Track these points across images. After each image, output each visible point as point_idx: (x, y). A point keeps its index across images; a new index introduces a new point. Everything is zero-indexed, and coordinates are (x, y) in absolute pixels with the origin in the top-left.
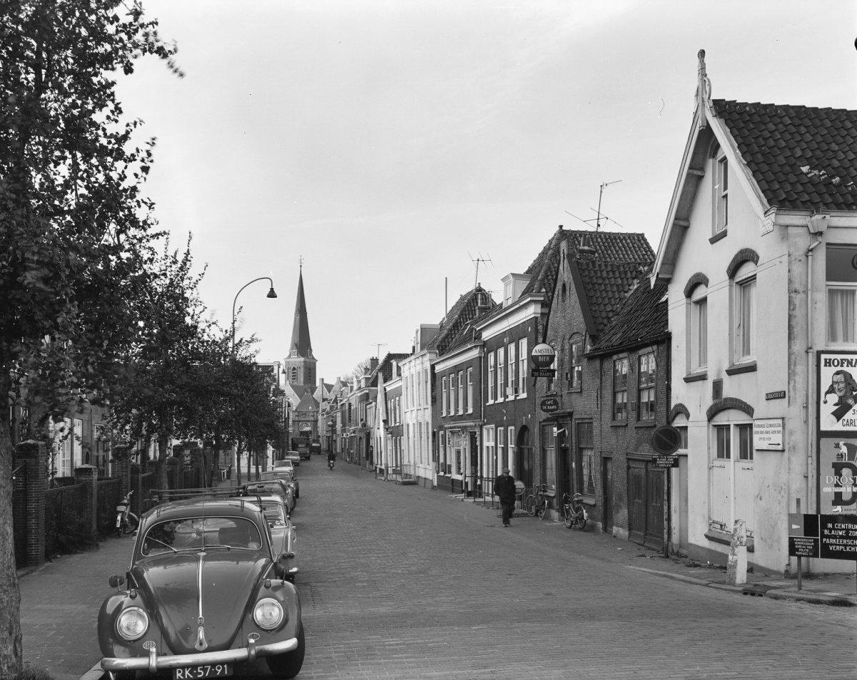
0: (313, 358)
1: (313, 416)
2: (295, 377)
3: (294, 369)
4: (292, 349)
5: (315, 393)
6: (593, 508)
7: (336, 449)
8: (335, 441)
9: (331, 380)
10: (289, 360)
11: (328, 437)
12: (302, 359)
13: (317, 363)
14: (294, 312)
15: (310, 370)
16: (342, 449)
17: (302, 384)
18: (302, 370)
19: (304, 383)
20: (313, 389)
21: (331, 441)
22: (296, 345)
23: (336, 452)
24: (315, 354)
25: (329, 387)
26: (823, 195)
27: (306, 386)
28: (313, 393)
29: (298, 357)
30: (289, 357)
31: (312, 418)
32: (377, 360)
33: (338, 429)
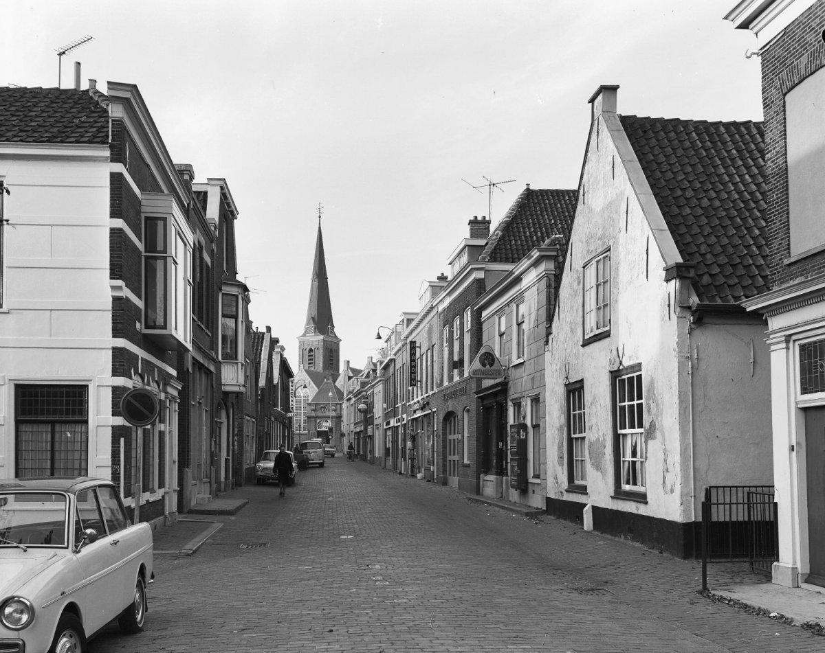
0: (336, 337)
1: (335, 410)
2: (311, 361)
3: (311, 350)
4: (308, 324)
5: (338, 381)
6: (467, 468)
7: (372, 451)
8: (371, 437)
9: (361, 364)
10: (305, 339)
11: (358, 433)
12: (321, 337)
13: (341, 343)
14: (311, 277)
15: (332, 353)
16: (387, 450)
17: (321, 370)
18: (321, 351)
19: (324, 368)
20: (335, 377)
21: (364, 438)
22: (313, 319)
23: (374, 457)
24: (339, 331)
25: (356, 372)
26: (703, 227)
27: (327, 372)
28: (334, 381)
29: (316, 335)
30: (304, 335)
31: (334, 414)
32: (485, 223)
33: (376, 416)
